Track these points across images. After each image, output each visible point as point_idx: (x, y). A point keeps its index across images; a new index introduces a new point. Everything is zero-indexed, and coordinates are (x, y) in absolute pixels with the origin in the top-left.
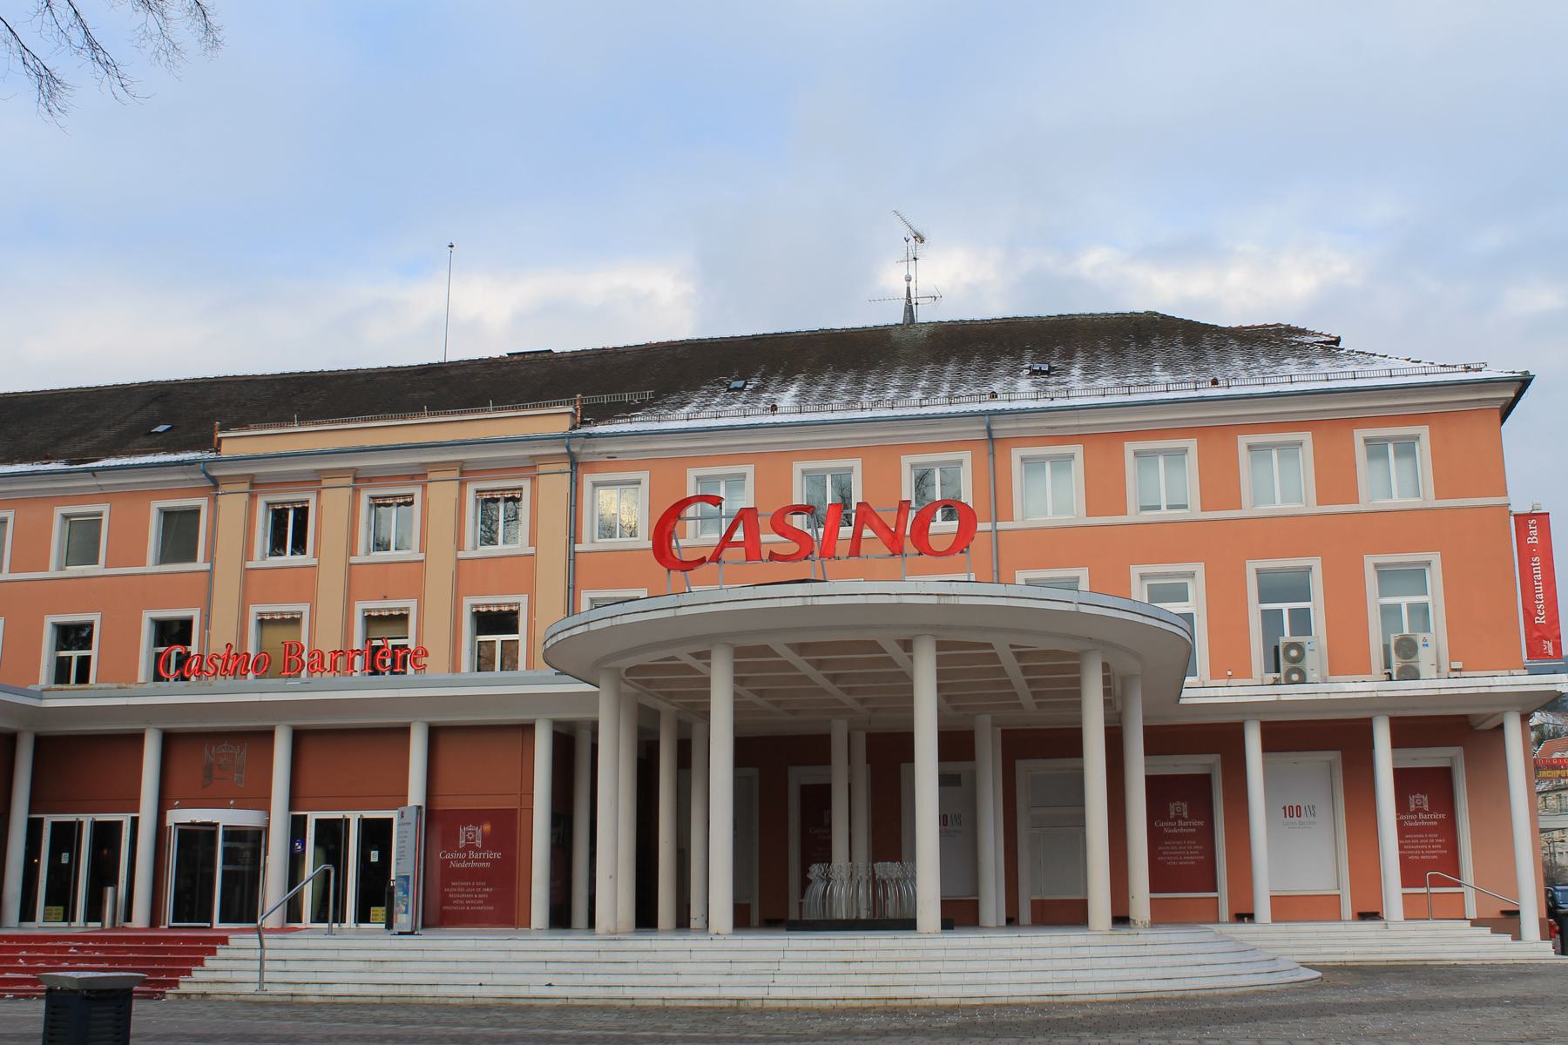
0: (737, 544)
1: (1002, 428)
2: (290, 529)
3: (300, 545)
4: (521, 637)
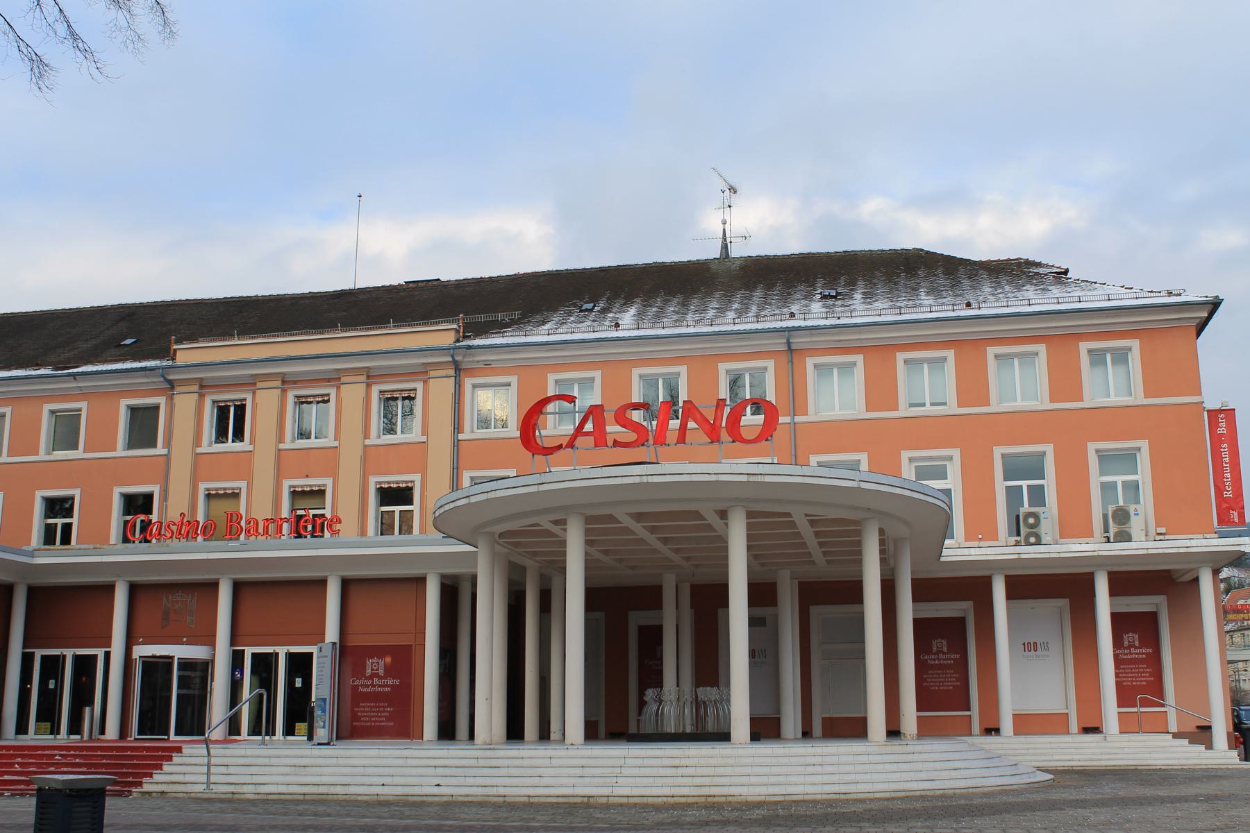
0: (588, 434)
1: (799, 341)
2: (231, 422)
3: (239, 435)
4: (415, 508)
